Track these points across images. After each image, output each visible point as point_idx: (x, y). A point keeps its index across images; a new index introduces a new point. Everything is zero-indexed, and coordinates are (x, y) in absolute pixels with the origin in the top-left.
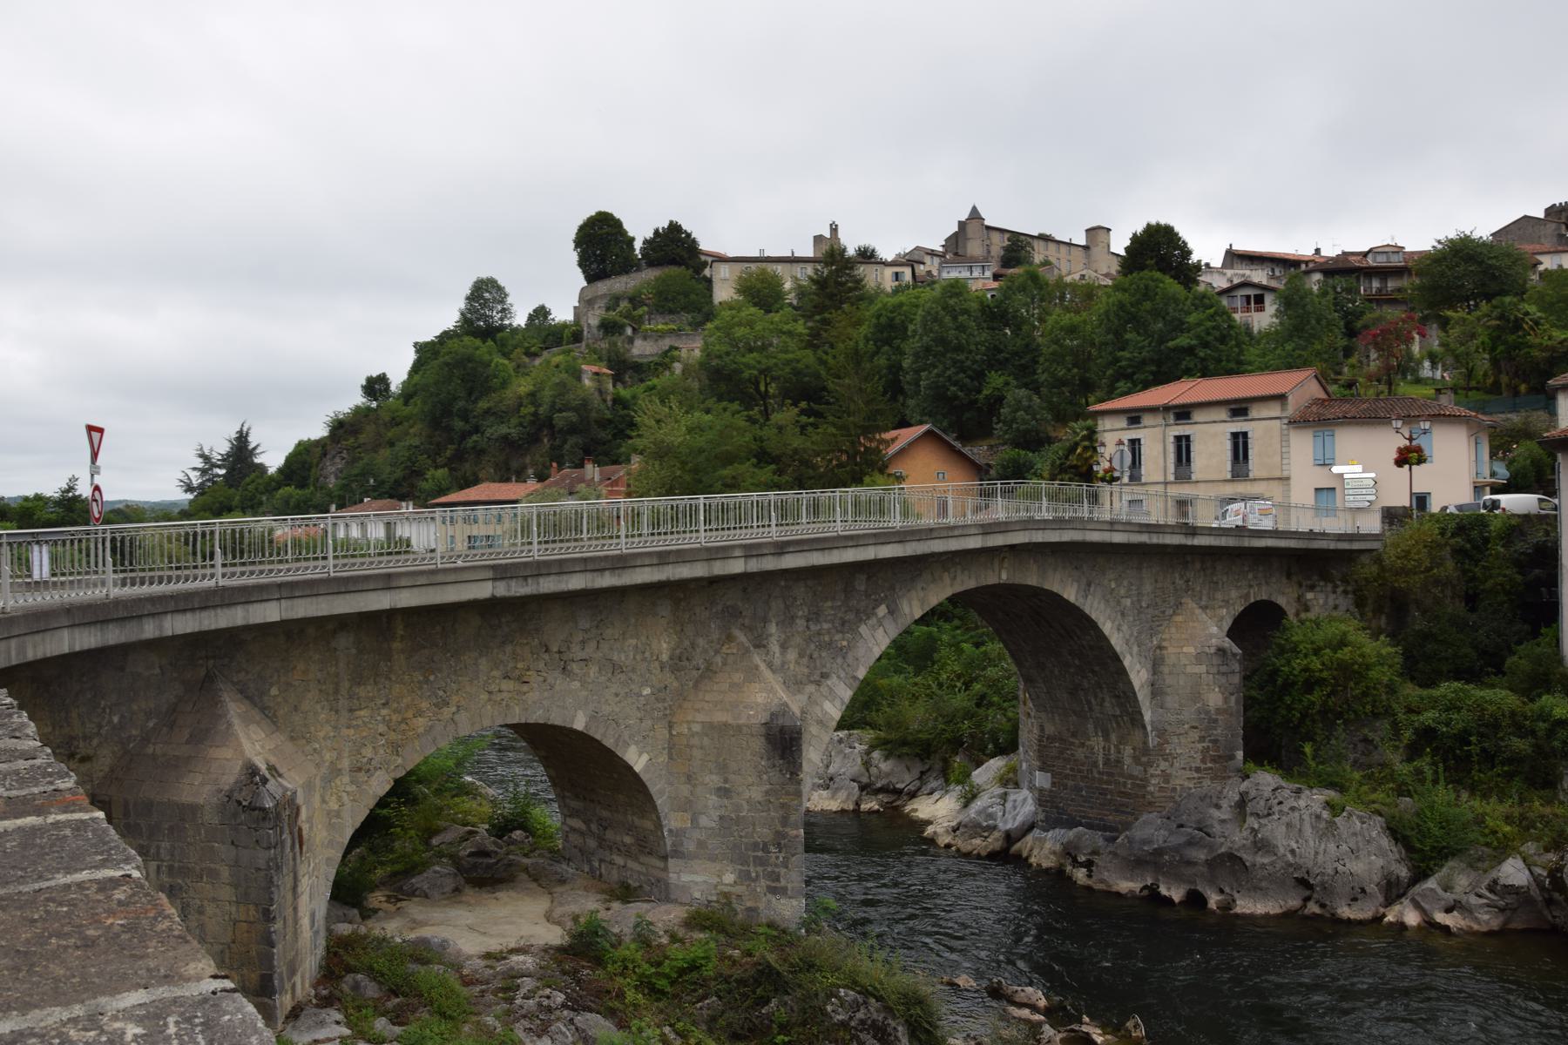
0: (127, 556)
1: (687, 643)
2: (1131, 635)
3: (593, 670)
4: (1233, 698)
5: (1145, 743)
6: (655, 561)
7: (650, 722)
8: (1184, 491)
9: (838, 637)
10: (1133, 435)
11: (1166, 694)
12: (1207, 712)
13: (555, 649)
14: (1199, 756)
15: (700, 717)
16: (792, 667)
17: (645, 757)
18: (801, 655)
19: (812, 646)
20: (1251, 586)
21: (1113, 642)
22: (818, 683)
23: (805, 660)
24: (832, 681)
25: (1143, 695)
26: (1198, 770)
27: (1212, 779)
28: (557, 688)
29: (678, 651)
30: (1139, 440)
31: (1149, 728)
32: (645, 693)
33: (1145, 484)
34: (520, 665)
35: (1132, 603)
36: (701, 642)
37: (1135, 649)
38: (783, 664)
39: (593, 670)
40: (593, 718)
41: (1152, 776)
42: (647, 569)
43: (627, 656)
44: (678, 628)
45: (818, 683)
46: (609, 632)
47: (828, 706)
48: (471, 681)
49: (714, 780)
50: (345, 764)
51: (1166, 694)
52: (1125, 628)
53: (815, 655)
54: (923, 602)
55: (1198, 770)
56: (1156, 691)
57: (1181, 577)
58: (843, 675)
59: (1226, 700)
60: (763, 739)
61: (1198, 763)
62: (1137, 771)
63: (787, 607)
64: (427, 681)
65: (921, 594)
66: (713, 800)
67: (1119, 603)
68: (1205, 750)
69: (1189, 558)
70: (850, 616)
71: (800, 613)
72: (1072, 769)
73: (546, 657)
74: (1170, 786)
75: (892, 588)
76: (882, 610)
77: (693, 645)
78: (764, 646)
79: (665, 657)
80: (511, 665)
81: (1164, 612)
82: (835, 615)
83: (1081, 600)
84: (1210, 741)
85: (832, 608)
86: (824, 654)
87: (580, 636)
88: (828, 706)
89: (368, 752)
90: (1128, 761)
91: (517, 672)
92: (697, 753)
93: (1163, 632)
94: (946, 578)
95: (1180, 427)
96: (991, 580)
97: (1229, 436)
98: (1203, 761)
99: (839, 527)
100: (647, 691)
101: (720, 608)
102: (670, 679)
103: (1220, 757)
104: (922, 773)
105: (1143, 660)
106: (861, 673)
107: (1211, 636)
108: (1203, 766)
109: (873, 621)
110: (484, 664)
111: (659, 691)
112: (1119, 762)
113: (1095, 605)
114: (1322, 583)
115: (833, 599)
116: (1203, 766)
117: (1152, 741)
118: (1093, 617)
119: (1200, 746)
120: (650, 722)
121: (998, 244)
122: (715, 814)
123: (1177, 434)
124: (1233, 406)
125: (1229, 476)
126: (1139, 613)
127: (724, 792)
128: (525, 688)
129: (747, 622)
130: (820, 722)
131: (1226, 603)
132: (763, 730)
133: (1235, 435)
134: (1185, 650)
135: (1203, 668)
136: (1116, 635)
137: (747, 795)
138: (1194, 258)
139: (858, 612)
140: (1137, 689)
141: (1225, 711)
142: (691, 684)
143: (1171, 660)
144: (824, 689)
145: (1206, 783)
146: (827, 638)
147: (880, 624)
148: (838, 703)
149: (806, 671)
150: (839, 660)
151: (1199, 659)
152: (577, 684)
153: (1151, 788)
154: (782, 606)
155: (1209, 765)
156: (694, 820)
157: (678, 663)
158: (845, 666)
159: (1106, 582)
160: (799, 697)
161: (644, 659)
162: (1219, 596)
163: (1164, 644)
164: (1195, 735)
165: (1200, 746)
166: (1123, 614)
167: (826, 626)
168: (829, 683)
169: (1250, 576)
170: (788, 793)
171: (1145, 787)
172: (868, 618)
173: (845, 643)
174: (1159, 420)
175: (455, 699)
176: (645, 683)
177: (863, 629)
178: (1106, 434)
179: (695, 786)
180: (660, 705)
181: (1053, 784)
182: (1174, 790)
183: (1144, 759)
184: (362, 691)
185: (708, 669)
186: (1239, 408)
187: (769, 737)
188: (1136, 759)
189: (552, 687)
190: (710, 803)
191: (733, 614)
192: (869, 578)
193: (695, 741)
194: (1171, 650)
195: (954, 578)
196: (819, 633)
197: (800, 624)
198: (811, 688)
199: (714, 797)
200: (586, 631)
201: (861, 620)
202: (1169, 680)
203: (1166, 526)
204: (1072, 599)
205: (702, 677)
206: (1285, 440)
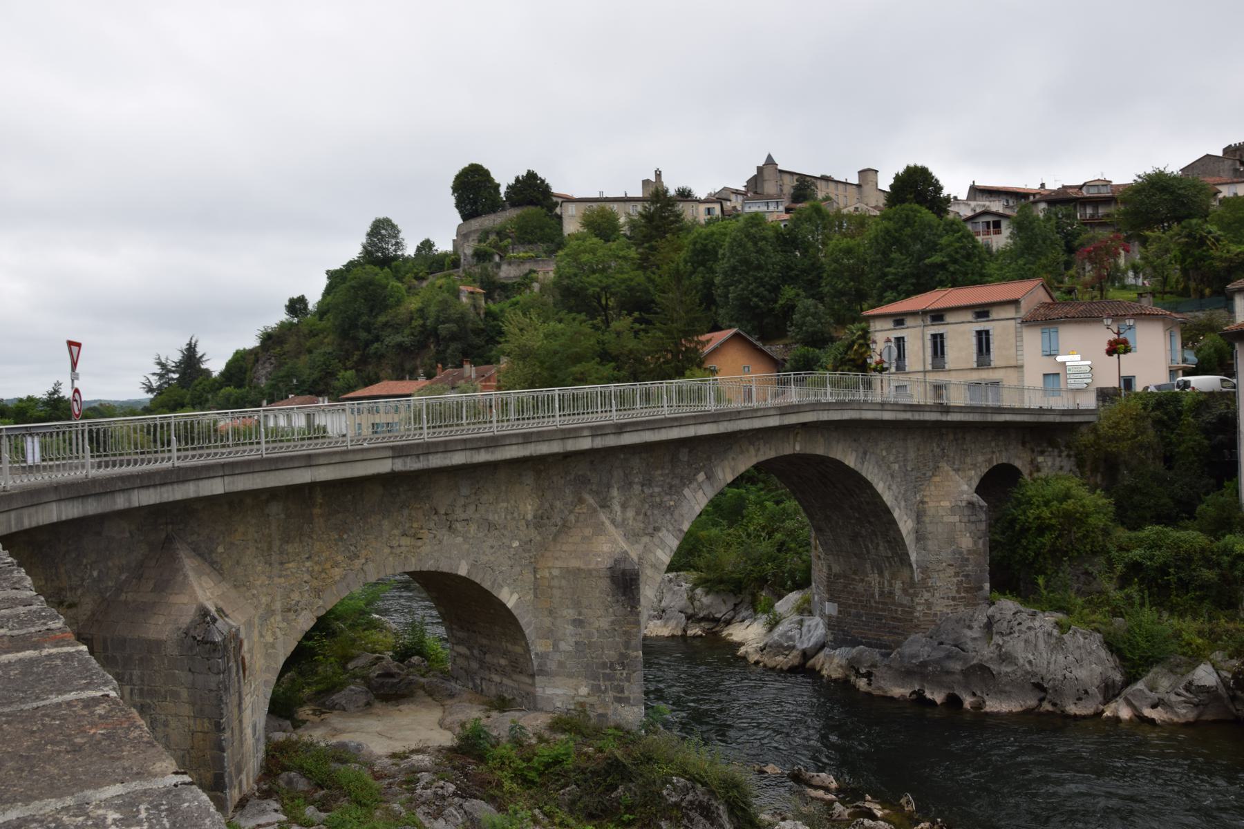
0: (102, 444)
1: (547, 505)
2: (899, 493)
3: (473, 528)
4: (981, 542)
5: (912, 578)
7: (519, 569)
8: (940, 377)
9: (666, 498)
10: (899, 334)
12: (961, 553)
13: (442, 512)
14: (954, 588)
15: (558, 564)
17: (516, 596)
18: (638, 513)
19: (647, 506)
20: (993, 452)
22: (652, 535)
23: (641, 517)
24: (663, 533)
25: (909, 540)
26: (954, 599)
28: (445, 542)
29: (540, 512)
30: (903, 338)
31: (915, 566)
32: (514, 545)
34: (415, 525)
35: (900, 467)
36: (558, 504)
37: (903, 503)
38: (624, 520)
39: (473, 528)
40: (474, 565)
41: (918, 604)
43: (499, 517)
44: (540, 494)
45: (652, 535)
46: (485, 498)
48: (376, 538)
49: (570, 613)
50: (278, 605)
52: (894, 487)
54: (733, 470)
55: (954, 599)
56: (920, 537)
57: (938, 446)
58: (671, 528)
59: (975, 543)
60: (608, 580)
61: (954, 594)
62: (906, 600)
63: (626, 475)
66: (570, 629)
67: (889, 468)
69: (944, 431)
70: (676, 482)
71: (636, 480)
72: (854, 600)
73: (435, 518)
76: (701, 477)
77: (552, 507)
78: (609, 507)
79: (530, 517)
80: (407, 525)
81: (924, 474)
83: (859, 466)
84: (963, 576)
85: (662, 475)
86: (656, 512)
87: (462, 501)
88: (659, 553)
89: (296, 596)
90: (898, 593)
91: (413, 531)
92: (557, 593)
93: (924, 491)
95: (936, 327)
97: (974, 334)
98: (958, 592)
101: (572, 477)
102: (533, 534)
104: (736, 605)
105: (909, 512)
106: (686, 527)
108: (958, 596)
109: (694, 485)
110: (386, 524)
112: (891, 593)
115: (663, 468)
116: (958, 596)
117: (917, 576)
118: (869, 478)
119: (955, 580)
120: (519, 569)
121: (789, 184)
122: (572, 640)
123: (933, 332)
124: (977, 310)
125: (975, 366)
127: (578, 623)
128: (419, 543)
129: (594, 488)
130: (654, 566)
131: (974, 466)
132: (608, 573)
133: (979, 333)
134: (942, 504)
135: (957, 518)
137: (597, 625)
138: (945, 193)
139: (682, 478)
142: (551, 537)
143: (931, 512)
144: (656, 540)
148: (668, 551)
149: (642, 525)
150: (668, 517)
151: (953, 510)
153: (917, 614)
154: (622, 474)
155: (963, 595)
156: (555, 646)
157: (540, 521)
160: (636, 546)
161: (513, 519)
162: (968, 460)
163: (926, 499)
164: (951, 571)
165: (955, 580)
166: (892, 477)
167: (657, 490)
168: (660, 534)
169: (993, 444)
170: (629, 623)
172: (690, 483)
173: (672, 503)
174: (919, 322)
175: (364, 552)
177: (686, 492)
178: (877, 334)
179: (555, 618)
180: (526, 555)
181: (840, 612)
182: (935, 615)
183: (911, 591)
184: (290, 548)
185: (564, 525)
186: (982, 311)
188: (905, 591)
189: (440, 542)
190: (568, 632)
191: (583, 481)
192: (690, 452)
193: (555, 583)
194: (931, 504)
195: (759, 450)
196: (651, 496)
198: (646, 539)
199: (571, 627)
201: (684, 485)
202: (930, 528)
204: (852, 465)
205: (559, 532)
206: (1019, 336)
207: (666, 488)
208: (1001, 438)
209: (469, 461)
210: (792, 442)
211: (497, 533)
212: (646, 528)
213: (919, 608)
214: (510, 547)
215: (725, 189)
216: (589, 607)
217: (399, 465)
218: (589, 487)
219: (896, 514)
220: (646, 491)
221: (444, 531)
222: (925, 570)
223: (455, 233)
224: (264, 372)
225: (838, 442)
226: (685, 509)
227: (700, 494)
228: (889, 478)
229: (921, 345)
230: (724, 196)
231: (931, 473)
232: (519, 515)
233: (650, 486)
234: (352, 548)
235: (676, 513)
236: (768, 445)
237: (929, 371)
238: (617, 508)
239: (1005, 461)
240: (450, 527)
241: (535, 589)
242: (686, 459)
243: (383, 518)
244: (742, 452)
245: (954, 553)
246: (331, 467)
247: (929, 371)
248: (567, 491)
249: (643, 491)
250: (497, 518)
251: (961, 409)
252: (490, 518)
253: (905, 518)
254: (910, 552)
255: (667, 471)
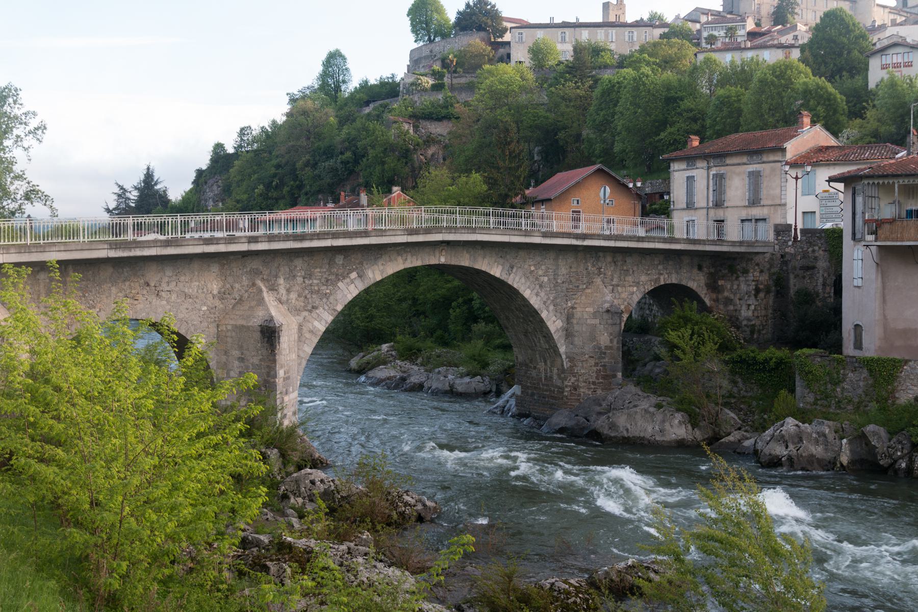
1: (228, 286)
2: (548, 299)
3: (174, 297)
5: (563, 365)
6: (202, 243)
7: (206, 324)
8: (720, 214)
11: (575, 336)
12: (600, 348)
13: (153, 285)
14: (594, 375)
15: (232, 322)
16: (293, 301)
18: (299, 296)
19: (307, 292)
21: (532, 302)
22: (310, 311)
27: (602, 390)
28: (154, 303)
29: (223, 290)
31: (564, 357)
32: (203, 309)
33: (696, 209)
34: (133, 291)
35: (549, 279)
36: (237, 286)
37: (551, 307)
38: (288, 300)
39: (174, 297)
41: (566, 386)
42: (191, 247)
43: (193, 291)
44: (223, 278)
45: (310, 311)
46: (182, 278)
47: (316, 323)
48: (107, 297)
49: (236, 353)
51: (575, 336)
52: (542, 294)
53: (309, 296)
54: (382, 272)
55: (594, 383)
56: (569, 334)
57: (593, 266)
58: (327, 308)
59: (611, 341)
60: (259, 333)
61: (594, 379)
62: (559, 383)
63: (291, 271)
64: (84, 296)
65: (381, 268)
66: (236, 363)
67: (537, 279)
68: (598, 371)
69: (601, 254)
71: (299, 274)
72: (530, 383)
73: (148, 288)
74: (577, 393)
75: (361, 263)
76: (354, 275)
78: (276, 290)
79: (215, 292)
80: (128, 291)
81: (578, 287)
82: (322, 276)
83: (506, 276)
84: (601, 366)
85: (320, 272)
87: (166, 279)
88: (316, 323)
90: (555, 377)
91: (132, 295)
92: (229, 340)
93: (577, 299)
94: (400, 259)
96: (433, 261)
98: (597, 378)
99: (352, 227)
100: (205, 308)
101: (248, 269)
102: (217, 303)
103: (607, 376)
105: (559, 315)
106: (339, 308)
107: (605, 302)
108: (597, 381)
109: (348, 280)
110: (114, 290)
111: (212, 309)
112: (551, 377)
113: (517, 279)
114: (729, 275)
115: (321, 267)
116: (597, 381)
118: (515, 286)
119: (595, 369)
120: (206, 324)
126: (555, 286)
127: (241, 360)
128: (136, 302)
129: (265, 277)
130: (311, 332)
131: (637, 284)
132: (259, 329)
133: (751, 174)
134: (587, 310)
135: (597, 321)
136: (535, 298)
137: (251, 361)
139: (337, 275)
140: (553, 332)
141: (611, 348)
142: (231, 307)
144: (314, 315)
145: (599, 392)
146: (316, 288)
147: (352, 282)
148: (323, 323)
149: (303, 304)
150: (324, 300)
151: (595, 315)
152: (164, 302)
153: (566, 394)
154: (287, 270)
155: (601, 380)
156: (228, 373)
158: (328, 303)
159: (526, 266)
160: (297, 317)
161: (203, 292)
162: (630, 279)
163: (575, 306)
164: (592, 362)
165: (595, 369)
166: (541, 286)
167: (315, 281)
168: (317, 311)
169: (660, 267)
170: (270, 360)
171: (563, 392)
172: (344, 279)
175: (99, 305)
176: (205, 304)
177: (340, 284)
178: (675, 173)
179: (228, 356)
180: (212, 316)
181: (522, 392)
182: (579, 395)
185: (240, 299)
187: (262, 332)
188: (559, 375)
189: (150, 303)
190: (235, 365)
191: (256, 273)
192: (344, 258)
193: (229, 334)
194: (579, 309)
195: (406, 259)
196: (311, 285)
197: (300, 280)
198: (306, 313)
200: (170, 277)
201: (339, 280)
202: (576, 328)
203: (708, 241)
204: (498, 275)
205: (237, 303)
207: (323, 280)
208: (670, 263)
209: (159, 254)
210: (437, 255)
211: (191, 300)
212: (306, 306)
213: (567, 389)
214: (200, 310)
215: (697, 10)
216: (248, 349)
217: (113, 254)
218: (261, 276)
219: (544, 315)
220: (307, 282)
221: (153, 296)
222: (571, 359)
223: (408, 58)
224: (212, 194)
225: (484, 258)
226: (339, 296)
227: (352, 287)
228: (538, 287)
229: (706, 184)
230: (694, 18)
231: (585, 286)
232: (208, 291)
233: (310, 278)
234: (91, 302)
235: (332, 298)
236: (415, 257)
237: (711, 208)
238: (282, 291)
239: (674, 281)
240: (158, 295)
241: (218, 338)
242: (341, 263)
243: (112, 286)
244: (391, 260)
245: (594, 347)
246: (68, 252)
247: (711, 208)
248: (244, 278)
249: (304, 282)
250: (191, 291)
251: (733, 243)
252: (186, 291)
253: (554, 318)
254: (559, 345)
255: (325, 270)
